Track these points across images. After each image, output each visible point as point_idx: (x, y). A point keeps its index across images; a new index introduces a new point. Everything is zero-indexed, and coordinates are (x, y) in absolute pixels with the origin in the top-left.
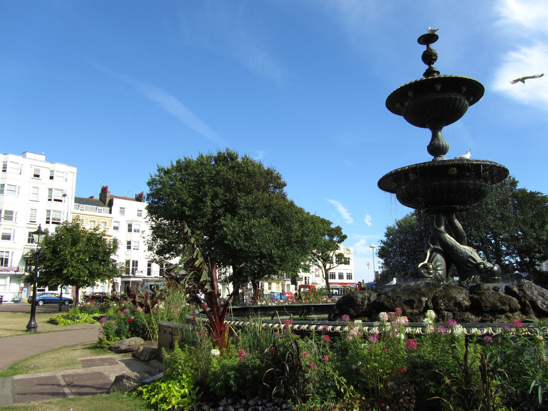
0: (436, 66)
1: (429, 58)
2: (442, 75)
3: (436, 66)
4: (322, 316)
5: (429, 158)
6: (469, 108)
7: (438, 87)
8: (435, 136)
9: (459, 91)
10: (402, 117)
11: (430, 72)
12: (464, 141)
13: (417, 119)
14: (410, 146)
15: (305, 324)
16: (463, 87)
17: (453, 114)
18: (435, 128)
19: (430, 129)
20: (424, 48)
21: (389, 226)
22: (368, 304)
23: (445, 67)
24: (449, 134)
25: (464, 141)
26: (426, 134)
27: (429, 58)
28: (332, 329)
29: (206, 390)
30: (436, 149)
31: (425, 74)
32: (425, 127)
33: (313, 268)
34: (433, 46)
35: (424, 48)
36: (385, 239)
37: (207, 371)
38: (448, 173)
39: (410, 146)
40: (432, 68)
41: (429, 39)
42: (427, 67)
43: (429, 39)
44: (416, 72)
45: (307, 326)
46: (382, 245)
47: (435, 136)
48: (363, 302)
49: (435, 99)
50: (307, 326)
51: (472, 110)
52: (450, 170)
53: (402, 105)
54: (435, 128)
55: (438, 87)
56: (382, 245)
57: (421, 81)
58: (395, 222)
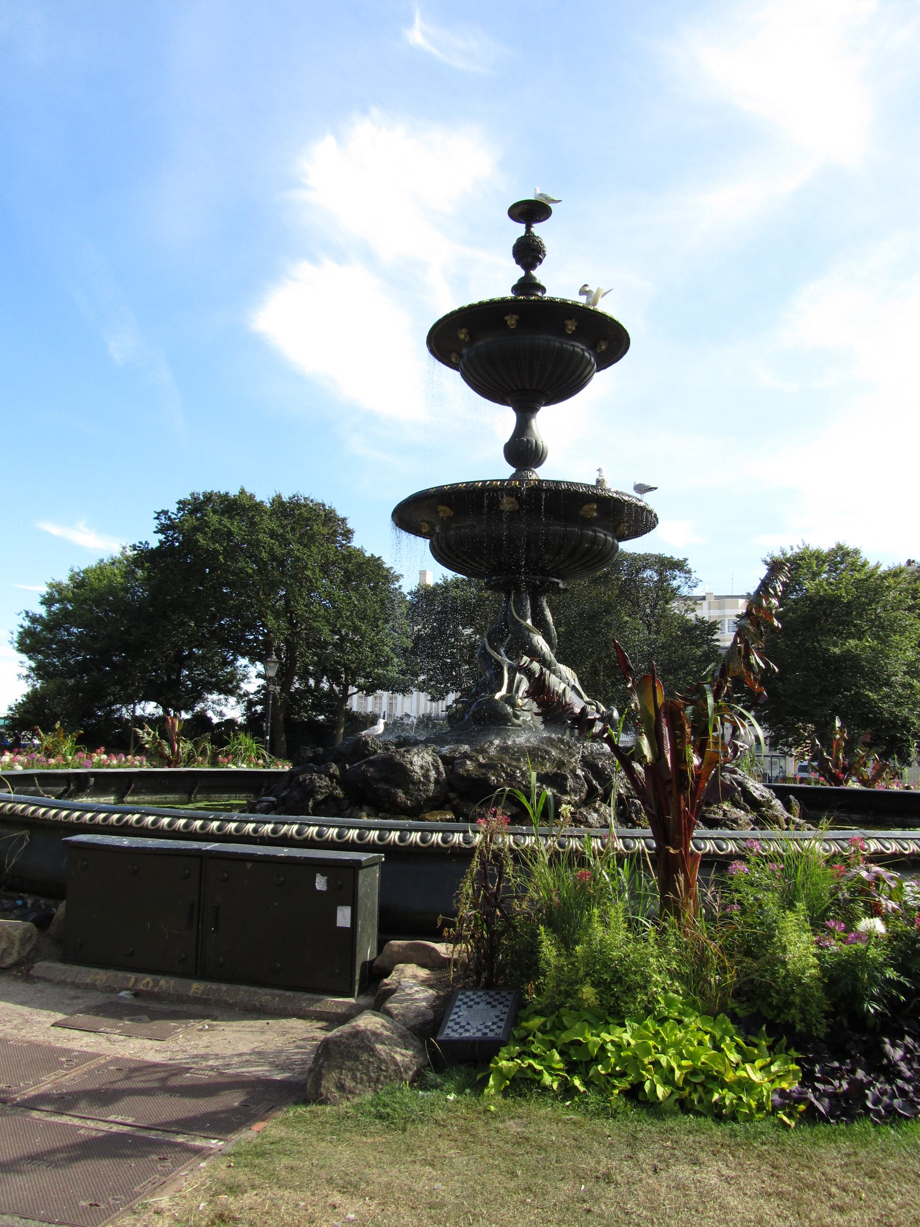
0: (540, 274)
1: (528, 253)
2: (548, 295)
3: (540, 274)
4: (102, 800)
5: (506, 471)
6: (596, 374)
8: (523, 426)
9: (561, 332)
10: (457, 374)
11: (527, 285)
12: (579, 441)
13: (489, 382)
14: (469, 438)
15: (134, 814)
16: (568, 322)
17: (564, 383)
19: (515, 409)
20: (519, 230)
21: (58, 580)
22: (437, 781)
23: (558, 281)
24: (549, 423)
25: (579, 441)
26: (503, 419)
27: (528, 253)
30: (522, 451)
32: (503, 402)
34: (538, 229)
35: (519, 230)
36: (42, 611)
38: (581, 513)
39: (469, 438)
41: (531, 211)
42: (521, 273)
43: (531, 211)
44: (498, 281)
45: (137, 816)
46: (27, 624)
47: (523, 426)
48: (426, 776)
50: (137, 816)
51: (602, 382)
52: (586, 507)
55: (571, 326)
56: (27, 624)
57: (503, 301)
58: (69, 574)
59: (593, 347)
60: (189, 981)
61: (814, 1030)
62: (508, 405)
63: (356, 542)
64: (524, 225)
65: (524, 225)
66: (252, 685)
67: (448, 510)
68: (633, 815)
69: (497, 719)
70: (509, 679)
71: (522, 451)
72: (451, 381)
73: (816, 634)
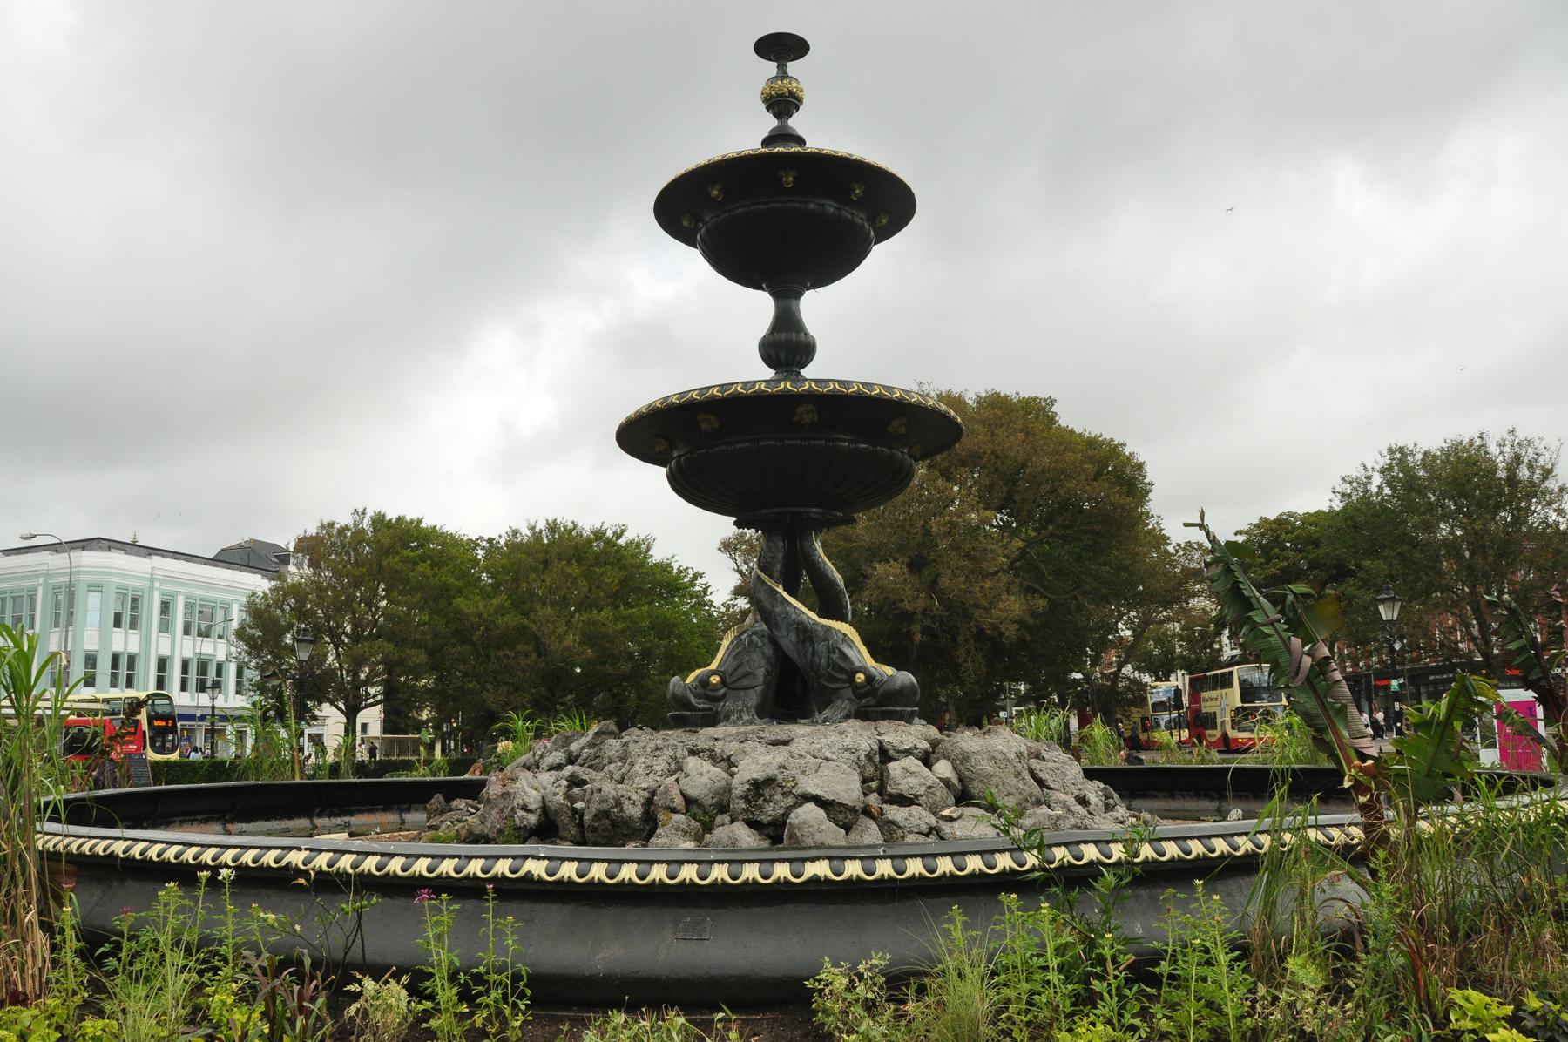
0: (796, 123)
1: (782, 103)
3: (796, 123)
7: (789, 180)
9: (844, 197)
11: (780, 136)
13: (738, 259)
14: (710, 328)
17: (836, 256)
23: (819, 132)
24: (818, 308)
25: (872, 328)
26: (758, 307)
27: (782, 103)
28: (355, 866)
29: (1566, 949)
30: (786, 345)
31: (767, 142)
39: (710, 328)
40: (787, 127)
42: (774, 123)
44: (745, 132)
49: (783, 214)
53: (697, 219)
55: (789, 180)
60: (149, 887)
61: (250, 742)
63: (660, 473)
67: (713, 418)
69: (1401, 775)
71: (786, 345)
72: (691, 263)
73: (1440, 578)
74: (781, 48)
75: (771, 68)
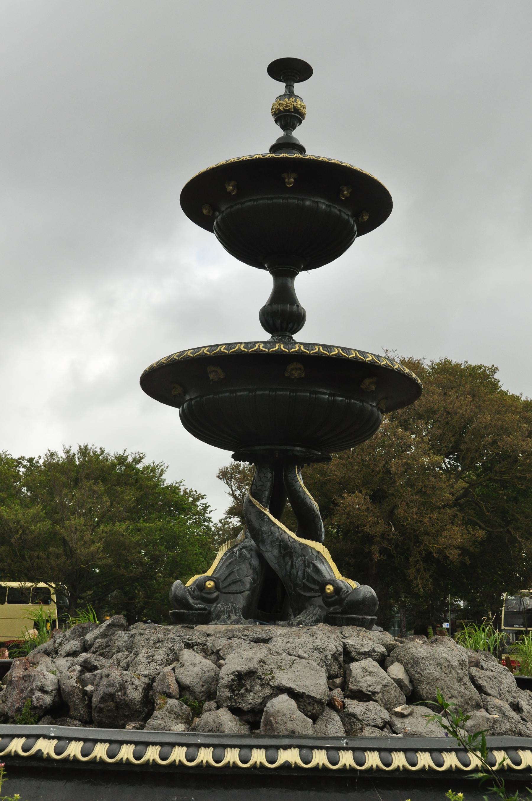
0: (299, 134)
1: (288, 117)
3: (299, 134)
11: (285, 144)
12: (348, 303)
13: (243, 245)
14: (218, 295)
17: (326, 246)
18: (284, 274)
23: (318, 142)
25: (348, 303)
26: (260, 283)
27: (288, 117)
30: (282, 314)
31: (274, 149)
32: (260, 266)
33: (456, 556)
35: (279, 87)
37: (470, 421)
39: (218, 295)
40: (292, 137)
44: (259, 141)
54: (284, 274)
59: (356, 215)
62: (265, 268)
64: (284, 84)
65: (284, 84)
66: (435, 555)
68: (258, 582)
70: (240, 392)
71: (282, 314)
74: (290, 70)
75: (280, 87)
